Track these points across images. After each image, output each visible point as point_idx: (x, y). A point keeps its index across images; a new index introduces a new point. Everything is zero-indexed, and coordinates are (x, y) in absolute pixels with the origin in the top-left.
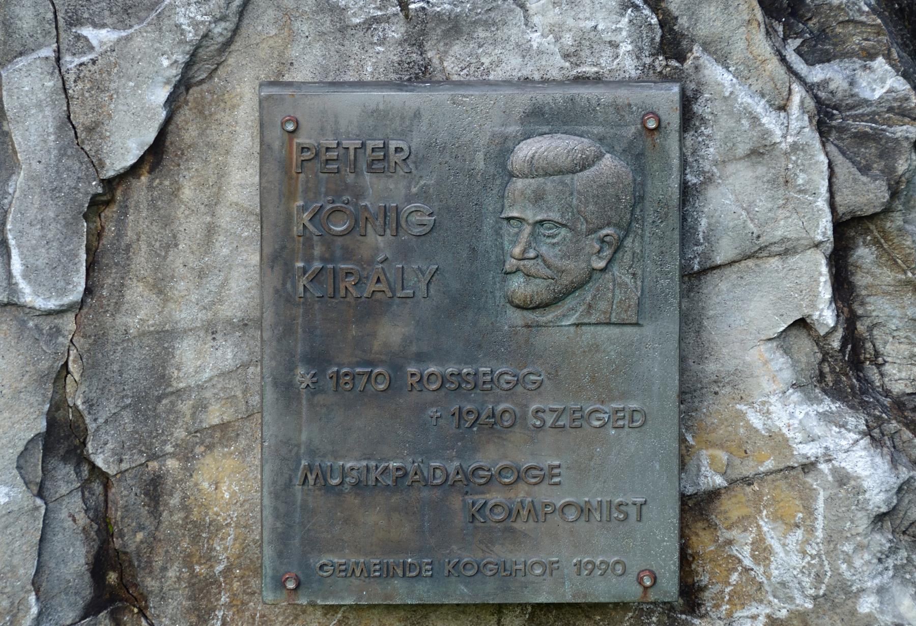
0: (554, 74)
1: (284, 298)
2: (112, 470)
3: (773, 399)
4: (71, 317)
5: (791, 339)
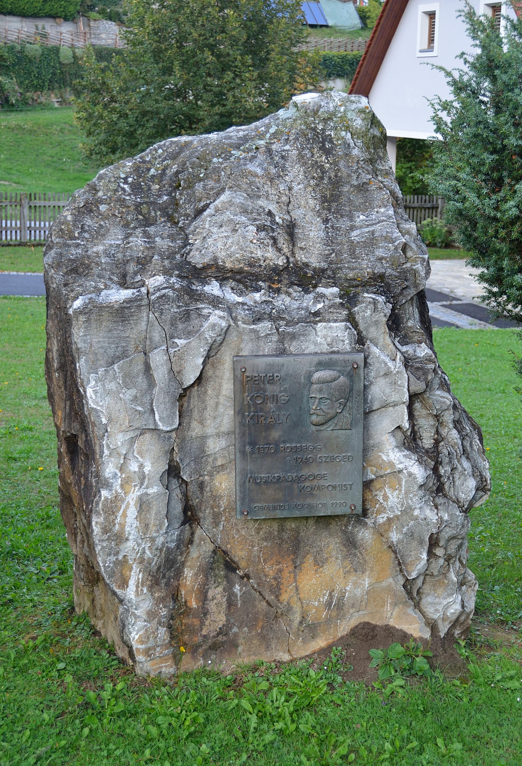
0: (325, 351)
1: (242, 424)
2: (188, 481)
3: (390, 451)
4: (174, 432)
5: (395, 433)
